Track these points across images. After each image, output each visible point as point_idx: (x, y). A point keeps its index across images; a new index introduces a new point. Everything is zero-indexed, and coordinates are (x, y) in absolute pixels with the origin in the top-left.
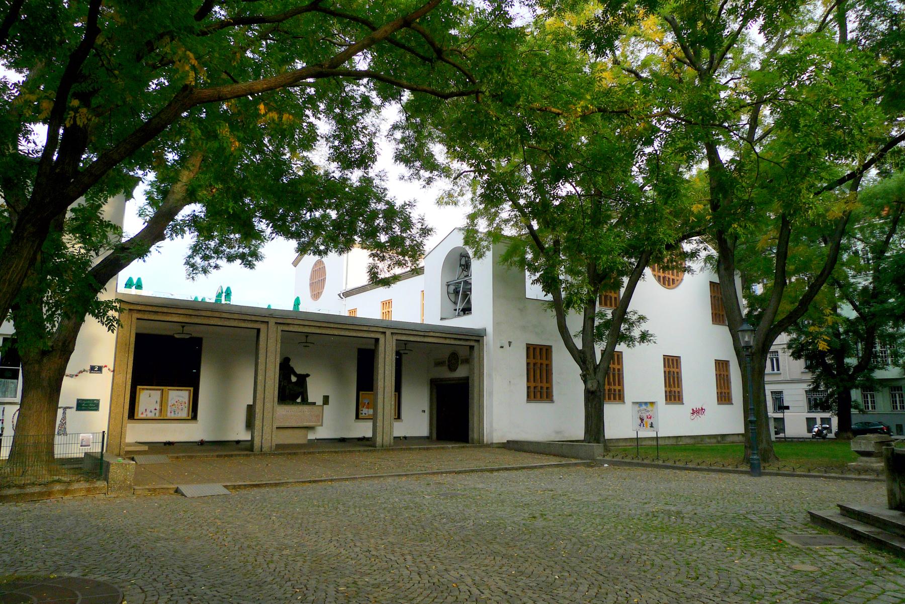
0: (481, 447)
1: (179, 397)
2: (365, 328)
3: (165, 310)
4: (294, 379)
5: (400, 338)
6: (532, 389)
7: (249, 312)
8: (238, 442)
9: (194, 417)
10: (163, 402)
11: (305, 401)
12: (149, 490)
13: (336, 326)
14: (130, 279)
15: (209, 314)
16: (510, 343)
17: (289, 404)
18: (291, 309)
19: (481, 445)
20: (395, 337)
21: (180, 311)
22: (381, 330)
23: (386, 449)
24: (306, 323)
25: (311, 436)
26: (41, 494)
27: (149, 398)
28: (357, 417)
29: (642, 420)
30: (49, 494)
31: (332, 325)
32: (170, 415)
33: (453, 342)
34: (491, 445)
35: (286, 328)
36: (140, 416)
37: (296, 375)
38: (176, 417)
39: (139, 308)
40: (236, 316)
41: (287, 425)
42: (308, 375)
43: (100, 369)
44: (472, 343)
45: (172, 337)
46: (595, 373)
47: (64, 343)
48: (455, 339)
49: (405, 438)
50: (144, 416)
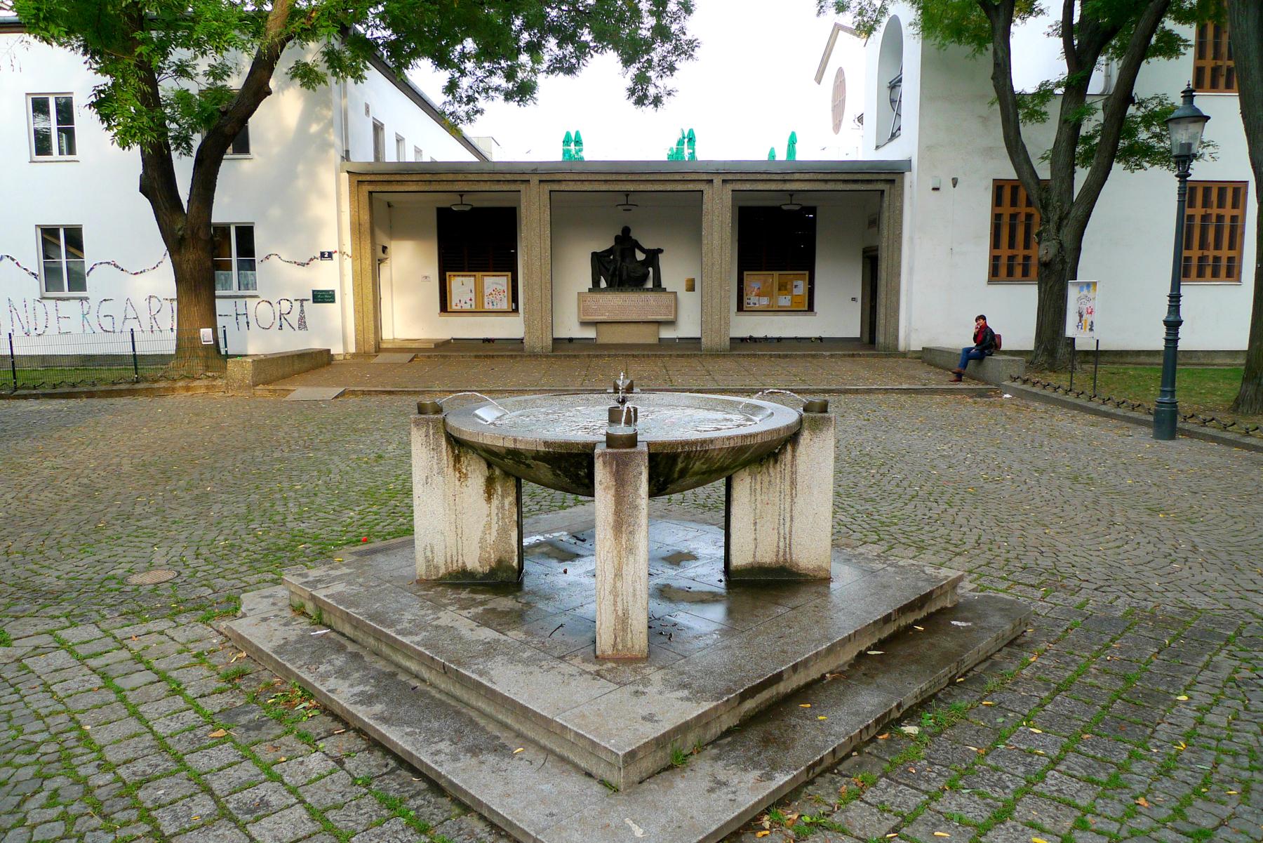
0: (888, 356)
1: (496, 284)
2: (677, 177)
3: (398, 178)
4: (640, 256)
5: (739, 186)
6: (1004, 261)
7: (503, 168)
8: (571, 340)
9: (516, 310)
10: (479, 291)
11: (658, 286)
12: (269, 391)
13: (630, 177)
14: (568, 134)
15: (451, 177)
16: (955, 182)
17: (626, 291)
18: (558, 157)
19: (893, 352)
20: (730, 187)
21: (415, 178)
22: (705, 177)
23: (716, 354)
24: (583, 177)
25: (666, 333)
26: (166, 389)
27: (462, 286)
28: (740, 308)
29: (1081, 316)
30: (173, 390)
31: (623, 177)
32: (487, 307)
33: (840, 187)
34: (904, 355)
35: (556, 187)
36: (454, 308)
37: (643, 250)
38: (495, 308)
39: (368, 178)
40: (486, 177)
41: (624, 318)
42: (660, 251)
43: (330, 255)
44: (880, 186)
45: (779, 208)
46: (1058, 229)
47: (193, 231)
48: (863, 181)
49: (821, 339)
50: (458, 308)
